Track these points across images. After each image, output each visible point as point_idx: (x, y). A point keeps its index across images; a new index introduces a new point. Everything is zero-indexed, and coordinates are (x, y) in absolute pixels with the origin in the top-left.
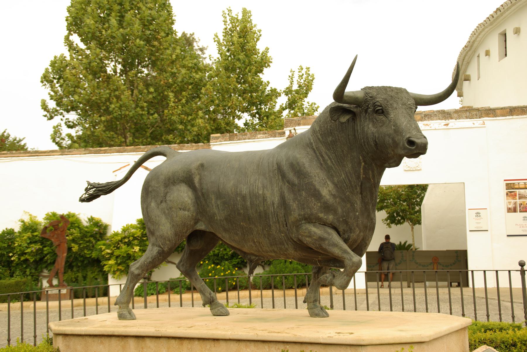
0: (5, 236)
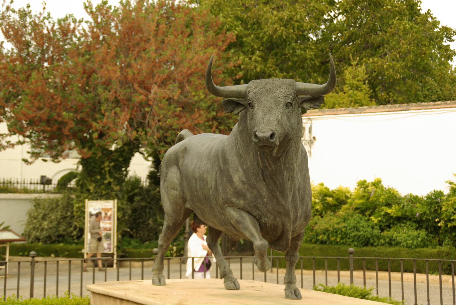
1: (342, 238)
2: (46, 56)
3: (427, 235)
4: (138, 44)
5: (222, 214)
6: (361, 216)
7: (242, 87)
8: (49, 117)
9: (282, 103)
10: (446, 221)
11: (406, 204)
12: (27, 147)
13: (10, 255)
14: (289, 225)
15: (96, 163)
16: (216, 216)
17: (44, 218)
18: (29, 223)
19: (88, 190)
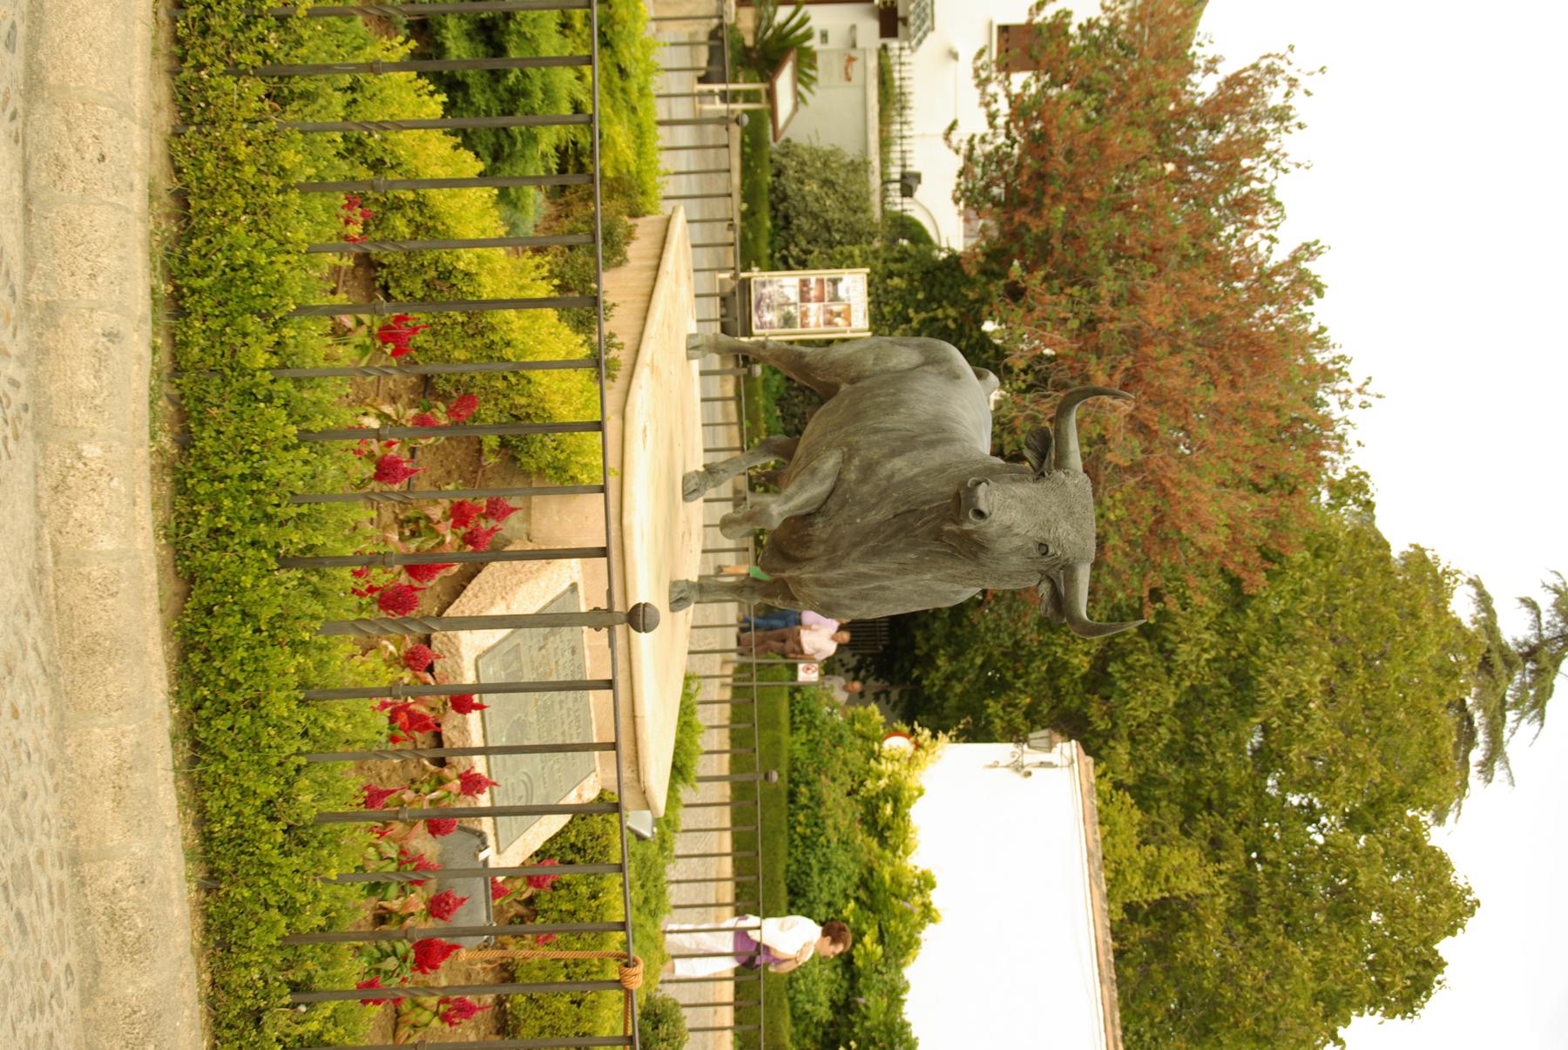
1: (803, 838)
3: (818, 1024)
4: (1227, 368)
6: (856, 879)
7: (1075, 460)
8: (1052, 177)
9: (1046, 536)
11: (886, 978)
16: (824, 435)
17: (827, 183)
18: (813, 152)
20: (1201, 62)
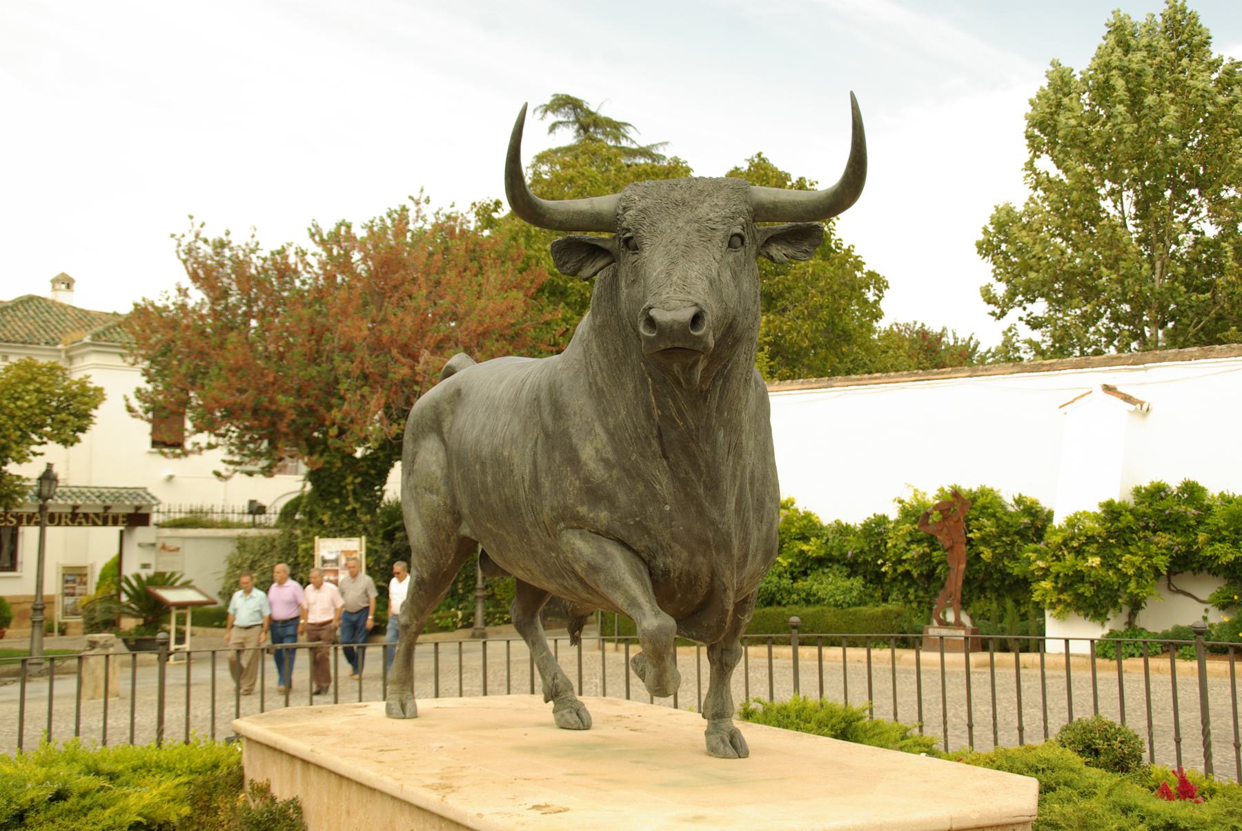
0: (873, 529)
2: (255, 309)
5: (550, 548)
9: (720, 235)
10: (893, 563)
12: (221, 453)
13: (193, 624)
14: (728, 573)
15: (332, 479)
19: (321, 522)
20: (180, 300)
